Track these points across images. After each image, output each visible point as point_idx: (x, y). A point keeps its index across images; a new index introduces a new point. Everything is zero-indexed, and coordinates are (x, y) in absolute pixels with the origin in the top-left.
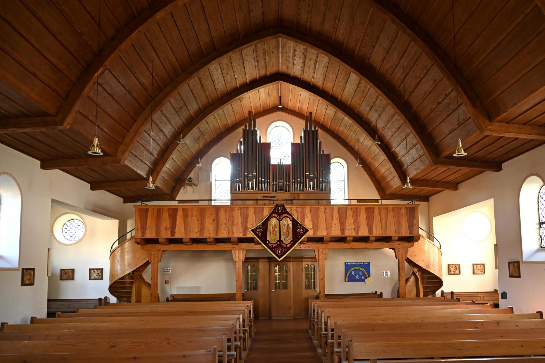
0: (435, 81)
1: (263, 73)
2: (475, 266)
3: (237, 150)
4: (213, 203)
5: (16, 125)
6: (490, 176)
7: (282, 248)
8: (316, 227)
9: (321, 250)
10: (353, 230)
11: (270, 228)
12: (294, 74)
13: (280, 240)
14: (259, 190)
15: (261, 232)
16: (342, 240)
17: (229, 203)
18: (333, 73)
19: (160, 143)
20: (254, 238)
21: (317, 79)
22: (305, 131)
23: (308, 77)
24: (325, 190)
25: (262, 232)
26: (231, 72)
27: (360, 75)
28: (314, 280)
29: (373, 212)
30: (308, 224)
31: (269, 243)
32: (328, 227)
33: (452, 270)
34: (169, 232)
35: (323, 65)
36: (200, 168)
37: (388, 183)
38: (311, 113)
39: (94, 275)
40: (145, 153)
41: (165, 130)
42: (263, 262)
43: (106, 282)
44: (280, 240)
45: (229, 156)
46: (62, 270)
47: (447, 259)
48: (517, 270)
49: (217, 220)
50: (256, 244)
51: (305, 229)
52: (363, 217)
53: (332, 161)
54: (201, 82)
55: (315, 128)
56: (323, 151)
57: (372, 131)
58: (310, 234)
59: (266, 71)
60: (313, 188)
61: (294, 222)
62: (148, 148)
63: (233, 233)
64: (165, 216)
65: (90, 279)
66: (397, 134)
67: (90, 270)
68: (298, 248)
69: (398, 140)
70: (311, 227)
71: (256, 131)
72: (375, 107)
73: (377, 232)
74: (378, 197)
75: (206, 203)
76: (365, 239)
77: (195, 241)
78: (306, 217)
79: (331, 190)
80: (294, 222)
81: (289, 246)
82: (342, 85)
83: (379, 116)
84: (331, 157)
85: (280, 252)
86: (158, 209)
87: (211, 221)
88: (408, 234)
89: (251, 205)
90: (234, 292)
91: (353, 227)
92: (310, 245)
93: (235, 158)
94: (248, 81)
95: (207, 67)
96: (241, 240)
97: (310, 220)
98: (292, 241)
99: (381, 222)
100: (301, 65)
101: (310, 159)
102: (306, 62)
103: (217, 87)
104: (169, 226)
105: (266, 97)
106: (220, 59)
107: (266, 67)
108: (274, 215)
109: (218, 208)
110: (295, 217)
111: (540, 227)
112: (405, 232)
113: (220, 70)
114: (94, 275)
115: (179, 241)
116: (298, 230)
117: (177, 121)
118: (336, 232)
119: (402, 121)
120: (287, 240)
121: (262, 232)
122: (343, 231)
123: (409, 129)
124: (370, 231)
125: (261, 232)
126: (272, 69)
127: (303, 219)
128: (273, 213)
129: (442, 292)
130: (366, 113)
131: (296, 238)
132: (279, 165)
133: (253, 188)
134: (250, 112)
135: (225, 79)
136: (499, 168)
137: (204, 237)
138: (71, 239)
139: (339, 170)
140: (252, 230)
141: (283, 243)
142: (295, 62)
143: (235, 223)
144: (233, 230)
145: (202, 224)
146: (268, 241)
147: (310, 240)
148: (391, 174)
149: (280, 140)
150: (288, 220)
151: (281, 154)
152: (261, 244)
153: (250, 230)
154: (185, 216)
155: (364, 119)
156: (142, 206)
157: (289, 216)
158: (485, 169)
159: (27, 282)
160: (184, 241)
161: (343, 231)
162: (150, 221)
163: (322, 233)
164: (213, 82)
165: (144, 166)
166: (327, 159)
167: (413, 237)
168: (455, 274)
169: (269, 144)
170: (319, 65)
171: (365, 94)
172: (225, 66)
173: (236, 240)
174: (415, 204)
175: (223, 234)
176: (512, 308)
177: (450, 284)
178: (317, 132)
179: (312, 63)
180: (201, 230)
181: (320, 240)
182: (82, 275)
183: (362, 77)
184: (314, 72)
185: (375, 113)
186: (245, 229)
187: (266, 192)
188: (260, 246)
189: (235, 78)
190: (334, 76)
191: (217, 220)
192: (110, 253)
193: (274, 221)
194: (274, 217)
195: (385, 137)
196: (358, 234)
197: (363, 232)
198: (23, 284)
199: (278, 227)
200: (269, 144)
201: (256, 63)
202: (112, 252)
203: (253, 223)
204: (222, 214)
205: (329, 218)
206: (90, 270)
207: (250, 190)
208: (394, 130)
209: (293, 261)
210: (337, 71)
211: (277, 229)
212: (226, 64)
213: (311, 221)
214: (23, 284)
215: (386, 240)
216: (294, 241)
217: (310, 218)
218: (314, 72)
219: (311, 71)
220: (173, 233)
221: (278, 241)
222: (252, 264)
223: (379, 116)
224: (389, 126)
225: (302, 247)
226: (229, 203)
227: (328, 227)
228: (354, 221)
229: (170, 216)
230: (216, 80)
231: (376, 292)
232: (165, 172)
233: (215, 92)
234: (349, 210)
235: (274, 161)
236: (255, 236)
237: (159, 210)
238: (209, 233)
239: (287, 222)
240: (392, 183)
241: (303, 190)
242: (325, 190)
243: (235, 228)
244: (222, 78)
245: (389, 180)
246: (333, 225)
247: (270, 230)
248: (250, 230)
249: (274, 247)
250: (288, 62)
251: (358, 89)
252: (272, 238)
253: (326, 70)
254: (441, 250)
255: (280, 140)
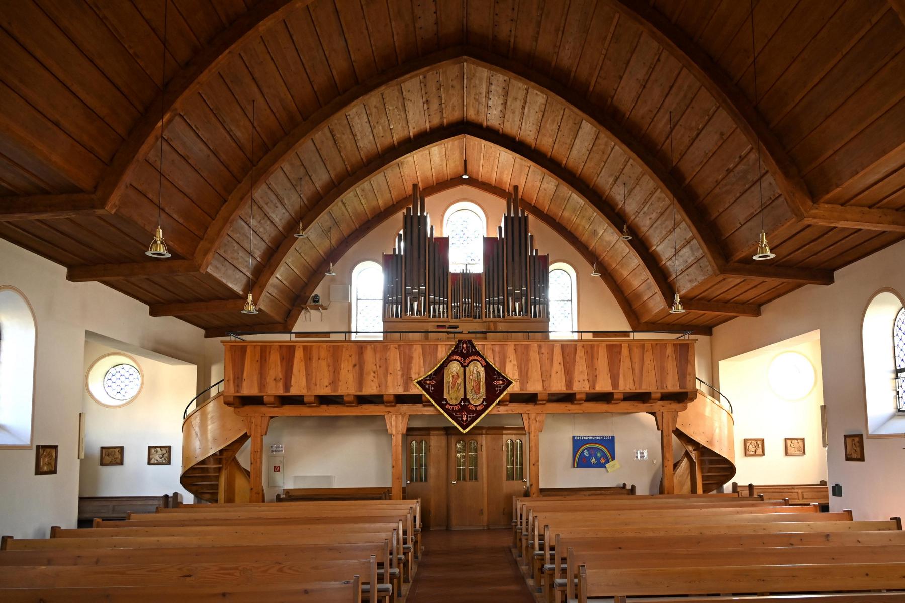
0: (722, 134)
1: (436, 121)
2: (789, 442)
3: (394, 250)
4: (354, 337)
5: (27, 208)
6: (814, 292)
7: (469, 411)
8: (524, 376)
9: (533, 416)
10: (587, 382)
11: (448, 379)
12: (489, 123)
13: (465, 399)
14: (430, 316)
15: (433, 386)
16: (568, 398)
17: (380, 337)
18: (553, 121)
19: (265, 238)
20: (421, 395)
21: (527, 131)
22: (506, 218)
23: (511, 127)
24: (540, 315)
25: (435, 385)
26: (383, 120)
27: (598, 125)
28: (522, 464)
29: (620, 352)
30: (511, 372)
31: (447, 403)
32: (545, 377)
33: (751, 448)
34: (280, 385)
35: (537, 109)
36: (333, 280)
37: (644, 304)
38: (516, 188)
39: (156, 457)
40: (241, 254)
41: (274, 216)
42: (437, 435)
43: (177, 468)
44: (465, 399)
45: (381, 259)
46: (102, 448)
47: (743, 431)
48: (858, 449)
49: (360, 366)
50: (425, 406)
51: (507, 380)
52: (602, 361)
53: (551, 268)
54: (333, 136)
55: (523, 213)
56: (537, 251)
57: (618, 218)
58: (515, 388)
59: (442, 117)
60: (520, 312)
61: (488, 368)
62: (246, 246)
63: (386, 387)
64: (275, 358)
65: (149, 463)
66: (658, 222)
67: (150, 448)
68: (494, 412)
69: (661, 233)
70: (517, 377)
71: (426, 217)
72: (623, 178)
73: (627, 385)
74: (627, 328)
75: (342, 337)
76: (606, 398)
77: (324, 400)
78: (508, 360)
79: (550, 316)
80: (488, 368)
81: (479, 408)
82: (568, 141)
83: (630, 192)
84: (550, 260)
85: (464, 419)
86: (262, 347)
87: (351, 368)
88: (677, 389)
89: (416, 341)
90: (389, 485)
91: (586, 378)
92: (515, 408)
93: (390, 262)
94: (411, 134)
95: (344, 111)
96: (400, 399)
97: (514, 365)
98: (484, 400)
99: (633, 370)
100: (500, 108)
101: (515, 263)
102: (509, 103)
103: (361, 144)
104: (280, 375)
105: (442, 160)
106: (366, 97)
107: (441, 112)
108: (454, 357)
109: (362, 345)
110: (490, 360)
111: (897, 378)
112: (672, 386)
113: (365, 116)
114: (156, 457)
115: (298, 401)
116: (495, 383)
117: (294, 201)
118: (558, 386)
119: (667, 201)
120: (476, 399)
121: (435, 385)
122: (569, 384)
123: (679, 214)
124: (615, 384)
125: (433, 386)
126: (451, 115)
127: (503, 364)
128: (453, 353)
129: (735, 485)
130: (607, 187)
131: (491, 396)
132: (463, 274)
133: (420, 311)
134: (415, 186)
135: (374, 131)
136: (828, 279)
137: (339, 393)
138: (119, 396)
139: (562, 283)
140: (419, 383)
141: (469, 403)
142: (491, 103)
143: (390, 370)
144: (386, 381)
145: (336, 371)
146: (446, 400)
147: (515, 398)
148: (649, 288)
149: (466, 233)
150: (479, 365)
151: (466, 256)
152: (433, 405)
153: (415, 382)
154: (308, 359)
155: (604, 198)
156: (235, 341)
157: (480, 359)
158: (805, 281)
159: (46, 469)
160: (306, 400)
161: (569, 384)
162: (250, 368)
163: (535, 387)
164: (354, 136)
165: (239, 275)
166: (543, 265)
167: (686, 393)
168: (755, 455)
169: (446, 240)
170: (529, 107)
171: (606, 157)
172: (374, 110)
173: (392, 399)
174: (688, 340)
175: (371, 389)
176: (850, 512)
177: (747, 472)
178: (526, 219)
179: (519, 104)
180: (335, 382)
181: (531, 399)
182: (135, 457)
183: (602, 128)
184: (522, 120)
185: (622, 187)
186: (407, 380)
187: (442, 319)
188: (432, 408)
189: (391, 130)
190: (555, 126)
191: (360, 366)
192: (182, 420)
193: (455, 367)
194: (455, 360)
195: (639, 228)
196: (594, 389)
197: (604, 386)
198: (39, 472)
199: (462, 377)
200: (446, 240)
201: (426, 105)
202: (187, 419)
203: (421, 370)
204: (369, 355)
205: (547, 362)
206: (150, 448)
207: (415, 316)
208: (654, 216)
209: (486, 434)
210: (560, 117)
211: (460, 381)
212: (375, 107)
213: (516, 368)
214: (39, 472)
215: (640, 398)
216: (489, 400)
217: (515, 363)
218: (522, 120)
219: (517, 118)
220: (287, 387)
221: (462, 400)
222: (419, 438)
223: (630, 192)
224: (645, 209)
225: (502, 409)
226: (380, 337)
227: (545, 377)
228: (588, 367)
229: (282, 359)
230: (358, 134)
231: (625, 485)
232: (274, 286)
233: (357, 153)
234: (579, 348)
235: (455, 267)
236: (424, 393)
237: (264, 349)
238: (348, 388)
239: (477, 369)
240: (651, 304)
241: (503, 316)
242: (540, 315)
243: (390, 378)
244: (369, 130)
245: (645, 298)
246: (553, 374)
247: (448, 382)
248: (415, 382)
249: (456, 411)
250: (479, 103)
251: (595, 148)
252: (452, 396)
253: (541, 116)
254: (733, 415)
255: (466, 233)
